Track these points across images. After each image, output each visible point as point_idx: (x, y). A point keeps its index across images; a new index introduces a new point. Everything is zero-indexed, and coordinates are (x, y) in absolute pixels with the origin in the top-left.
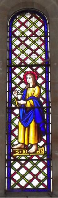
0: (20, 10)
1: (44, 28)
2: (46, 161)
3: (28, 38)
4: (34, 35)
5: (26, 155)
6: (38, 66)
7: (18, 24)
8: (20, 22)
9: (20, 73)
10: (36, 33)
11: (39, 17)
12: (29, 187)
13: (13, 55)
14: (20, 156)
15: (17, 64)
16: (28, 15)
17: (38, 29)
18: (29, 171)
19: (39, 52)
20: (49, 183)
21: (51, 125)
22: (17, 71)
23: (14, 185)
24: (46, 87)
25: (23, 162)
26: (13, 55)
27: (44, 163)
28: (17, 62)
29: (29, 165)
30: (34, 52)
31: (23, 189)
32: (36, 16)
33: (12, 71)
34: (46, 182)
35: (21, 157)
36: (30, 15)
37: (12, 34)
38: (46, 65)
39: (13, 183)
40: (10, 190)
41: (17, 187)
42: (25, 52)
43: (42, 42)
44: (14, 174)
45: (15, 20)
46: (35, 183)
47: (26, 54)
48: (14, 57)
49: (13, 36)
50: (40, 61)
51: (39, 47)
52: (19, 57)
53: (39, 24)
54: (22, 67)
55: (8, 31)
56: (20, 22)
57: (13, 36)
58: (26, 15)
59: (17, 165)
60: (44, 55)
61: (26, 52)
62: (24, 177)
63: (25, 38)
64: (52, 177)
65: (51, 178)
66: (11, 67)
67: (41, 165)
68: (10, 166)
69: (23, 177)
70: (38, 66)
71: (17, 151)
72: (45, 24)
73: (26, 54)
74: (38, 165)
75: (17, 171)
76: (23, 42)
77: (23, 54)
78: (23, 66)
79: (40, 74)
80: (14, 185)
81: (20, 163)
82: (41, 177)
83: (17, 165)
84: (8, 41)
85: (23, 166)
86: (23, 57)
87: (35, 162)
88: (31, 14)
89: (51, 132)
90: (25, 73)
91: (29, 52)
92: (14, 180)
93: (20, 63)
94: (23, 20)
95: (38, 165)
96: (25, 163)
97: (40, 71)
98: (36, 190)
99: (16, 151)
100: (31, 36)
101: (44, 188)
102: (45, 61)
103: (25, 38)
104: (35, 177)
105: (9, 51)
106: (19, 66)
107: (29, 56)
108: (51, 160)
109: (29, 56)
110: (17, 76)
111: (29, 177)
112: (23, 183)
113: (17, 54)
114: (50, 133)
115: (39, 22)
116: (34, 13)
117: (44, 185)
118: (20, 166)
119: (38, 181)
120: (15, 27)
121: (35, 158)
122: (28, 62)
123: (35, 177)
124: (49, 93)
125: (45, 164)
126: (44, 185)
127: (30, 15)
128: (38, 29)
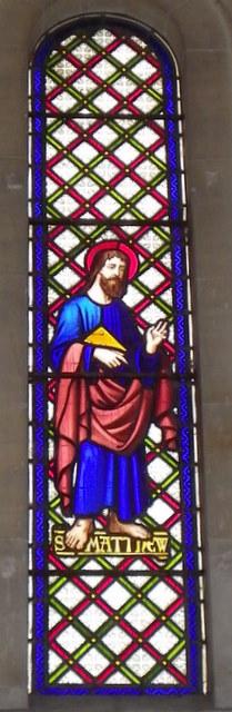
1: (169, 186)
3: (104, 119)
5: (103, 557)
6: (146, 225)
7: (66, 69)
8: (74, 61)
9: (76, 251)
12: (117, 679)
15: (66, 214)
16: (104, 38)
17: (143, 87)
18: (106, 153)
19: (164, 640)
21: (183, 176)
22: (67, 241)
24: (169, 192)
25: (93, 581)
27: (174, 586)
28: (66, 206)
29: (116, 595)
30: (127, 171)
31: (94, 687)
33: (44, 243)
34: (181, 663)
35: (84, 560)
36: (113, 38)
37: (42, 102)
39: (54, 661)
40: (45, 686)
41: (72, 678)
42: (92, 104)
43: (161, 278)
44: (60, 627)
45: (54, 52)
46: (141, 663)
47: (97, 180)
48: (51, 187)
49: (47, 111)
50: (149, 207)
51: (162, 618)
52: (71, 187)
53: (144, 70)
55: (30, 424)
56: (74, 61)
57: (47, 111)
58: (95, 38)
60: (183, 656)
61: (97, 170)
62: (93, 645)
64: (182, 168)
66: (45, 226)
67: (163, 595)
69: (94, 639)
70: (146, 225)
72: (165, 70)
73: (97, 180)
74: (151, 596)
76: (85, 136)
77: (86, 161)
78: (88, 223)
79: (143, 58)
81: (83, 587)
82: (147, 171)
84: (30, 239)
85: (93, 597)
86: (87, 189)
88: (113, 33)
89: (204, 637)
90: (91, 248)
91: (107, 171)
92: (61, 652)
93: (76, 211)
94: (83, 53)
95: (151, 596)
96: (102, 587)
97: (151, 242)
98: (142, 689)
101: (175, 682)
104: (140, 640)
105: (34, 201)
106: (72, 223)
107: (107, 188)
109: (107, 188)
110: (66, 187)
111: (117, 640)
112: (94, 663)
113: (66, 178)
118: (80, 596)
119: (158, 629)
120: (58, 611)
121: (138, 565)
122: (108, 207)
123: (140, 640)
125: (176, 591)
126: (173, 670)
127: (113, 38)
128: (143, 87)
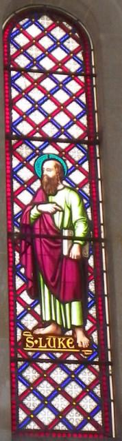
0: (25, 7)
2: (97, 367)
4: (60, 70)
10: (66, 65)
11: (70, 28)
13: (12, 46)
14: (36, 352)
20: (106, 418)
23: (27, 421)
26: (12, 46)
27: (94, 371)
32: (63, 25)
34: (98, 418)
38: (91, 140)
41: (32, 426)
53: (72, 44)
54: (41, 365)
59: (30, 374)
63: (39, 75)
65: (93, 67)
68: (16, 376)
71: (29, 339)
75: (24, 94)
80: (27, 421)
83: (30, 374)
87: (73, 367)
88: (52, 18)
92: (26, 409)
94: (34, 31)
99: (28, 341)
100: (53, 71)
102: (100, 354)
103: (39, 75)
108: (97, 144)
114: (96, 112)
115: (71, 39)
116: (58, 17)
117: (95, 424)
123: (74, 403)
124: (103, 275)
